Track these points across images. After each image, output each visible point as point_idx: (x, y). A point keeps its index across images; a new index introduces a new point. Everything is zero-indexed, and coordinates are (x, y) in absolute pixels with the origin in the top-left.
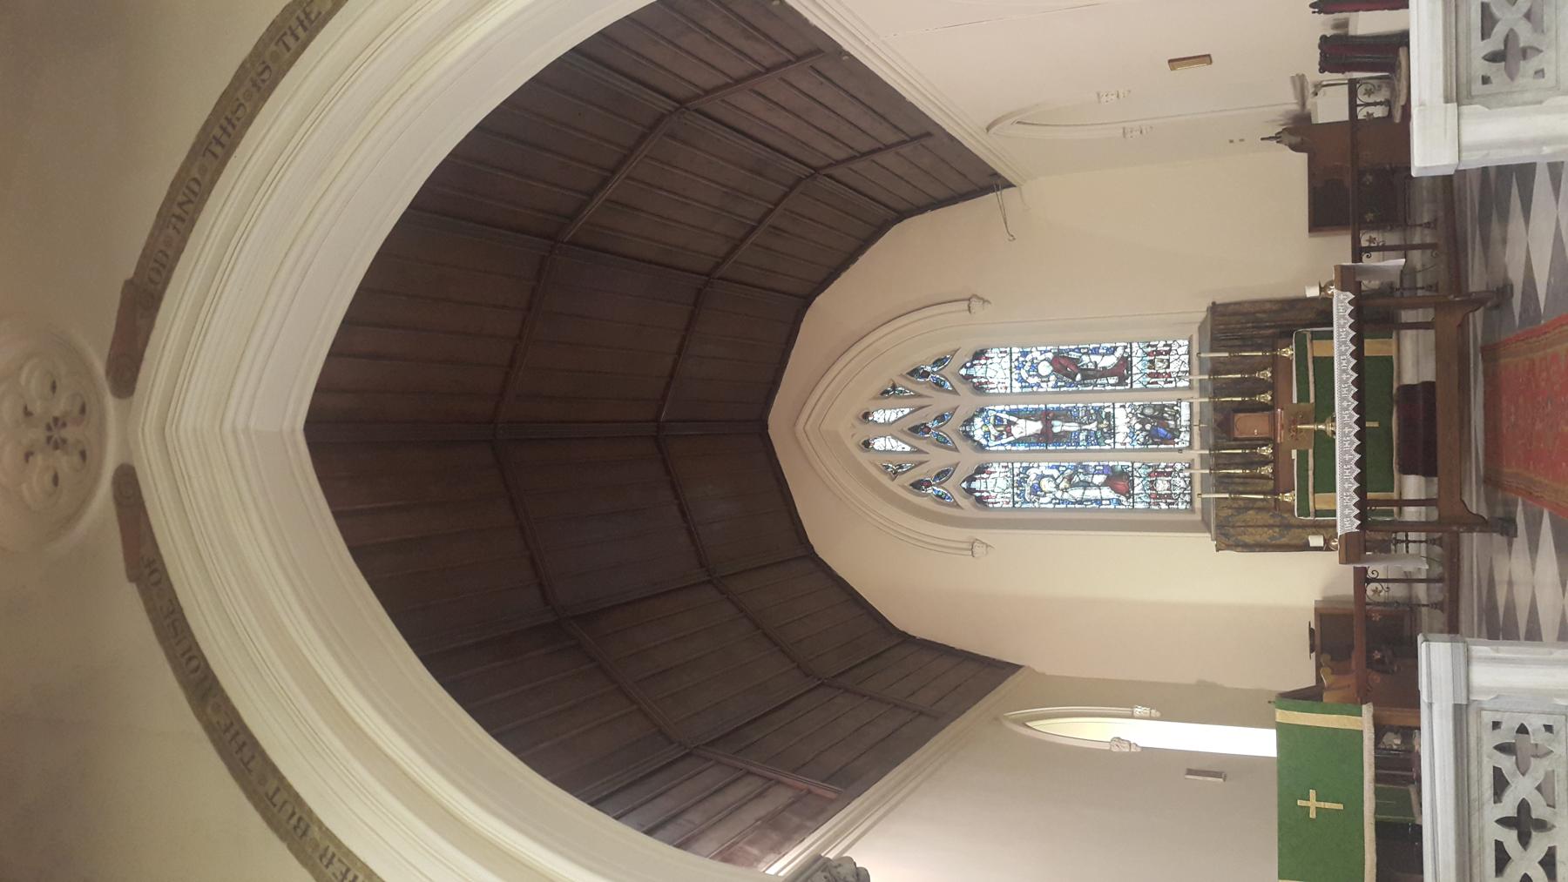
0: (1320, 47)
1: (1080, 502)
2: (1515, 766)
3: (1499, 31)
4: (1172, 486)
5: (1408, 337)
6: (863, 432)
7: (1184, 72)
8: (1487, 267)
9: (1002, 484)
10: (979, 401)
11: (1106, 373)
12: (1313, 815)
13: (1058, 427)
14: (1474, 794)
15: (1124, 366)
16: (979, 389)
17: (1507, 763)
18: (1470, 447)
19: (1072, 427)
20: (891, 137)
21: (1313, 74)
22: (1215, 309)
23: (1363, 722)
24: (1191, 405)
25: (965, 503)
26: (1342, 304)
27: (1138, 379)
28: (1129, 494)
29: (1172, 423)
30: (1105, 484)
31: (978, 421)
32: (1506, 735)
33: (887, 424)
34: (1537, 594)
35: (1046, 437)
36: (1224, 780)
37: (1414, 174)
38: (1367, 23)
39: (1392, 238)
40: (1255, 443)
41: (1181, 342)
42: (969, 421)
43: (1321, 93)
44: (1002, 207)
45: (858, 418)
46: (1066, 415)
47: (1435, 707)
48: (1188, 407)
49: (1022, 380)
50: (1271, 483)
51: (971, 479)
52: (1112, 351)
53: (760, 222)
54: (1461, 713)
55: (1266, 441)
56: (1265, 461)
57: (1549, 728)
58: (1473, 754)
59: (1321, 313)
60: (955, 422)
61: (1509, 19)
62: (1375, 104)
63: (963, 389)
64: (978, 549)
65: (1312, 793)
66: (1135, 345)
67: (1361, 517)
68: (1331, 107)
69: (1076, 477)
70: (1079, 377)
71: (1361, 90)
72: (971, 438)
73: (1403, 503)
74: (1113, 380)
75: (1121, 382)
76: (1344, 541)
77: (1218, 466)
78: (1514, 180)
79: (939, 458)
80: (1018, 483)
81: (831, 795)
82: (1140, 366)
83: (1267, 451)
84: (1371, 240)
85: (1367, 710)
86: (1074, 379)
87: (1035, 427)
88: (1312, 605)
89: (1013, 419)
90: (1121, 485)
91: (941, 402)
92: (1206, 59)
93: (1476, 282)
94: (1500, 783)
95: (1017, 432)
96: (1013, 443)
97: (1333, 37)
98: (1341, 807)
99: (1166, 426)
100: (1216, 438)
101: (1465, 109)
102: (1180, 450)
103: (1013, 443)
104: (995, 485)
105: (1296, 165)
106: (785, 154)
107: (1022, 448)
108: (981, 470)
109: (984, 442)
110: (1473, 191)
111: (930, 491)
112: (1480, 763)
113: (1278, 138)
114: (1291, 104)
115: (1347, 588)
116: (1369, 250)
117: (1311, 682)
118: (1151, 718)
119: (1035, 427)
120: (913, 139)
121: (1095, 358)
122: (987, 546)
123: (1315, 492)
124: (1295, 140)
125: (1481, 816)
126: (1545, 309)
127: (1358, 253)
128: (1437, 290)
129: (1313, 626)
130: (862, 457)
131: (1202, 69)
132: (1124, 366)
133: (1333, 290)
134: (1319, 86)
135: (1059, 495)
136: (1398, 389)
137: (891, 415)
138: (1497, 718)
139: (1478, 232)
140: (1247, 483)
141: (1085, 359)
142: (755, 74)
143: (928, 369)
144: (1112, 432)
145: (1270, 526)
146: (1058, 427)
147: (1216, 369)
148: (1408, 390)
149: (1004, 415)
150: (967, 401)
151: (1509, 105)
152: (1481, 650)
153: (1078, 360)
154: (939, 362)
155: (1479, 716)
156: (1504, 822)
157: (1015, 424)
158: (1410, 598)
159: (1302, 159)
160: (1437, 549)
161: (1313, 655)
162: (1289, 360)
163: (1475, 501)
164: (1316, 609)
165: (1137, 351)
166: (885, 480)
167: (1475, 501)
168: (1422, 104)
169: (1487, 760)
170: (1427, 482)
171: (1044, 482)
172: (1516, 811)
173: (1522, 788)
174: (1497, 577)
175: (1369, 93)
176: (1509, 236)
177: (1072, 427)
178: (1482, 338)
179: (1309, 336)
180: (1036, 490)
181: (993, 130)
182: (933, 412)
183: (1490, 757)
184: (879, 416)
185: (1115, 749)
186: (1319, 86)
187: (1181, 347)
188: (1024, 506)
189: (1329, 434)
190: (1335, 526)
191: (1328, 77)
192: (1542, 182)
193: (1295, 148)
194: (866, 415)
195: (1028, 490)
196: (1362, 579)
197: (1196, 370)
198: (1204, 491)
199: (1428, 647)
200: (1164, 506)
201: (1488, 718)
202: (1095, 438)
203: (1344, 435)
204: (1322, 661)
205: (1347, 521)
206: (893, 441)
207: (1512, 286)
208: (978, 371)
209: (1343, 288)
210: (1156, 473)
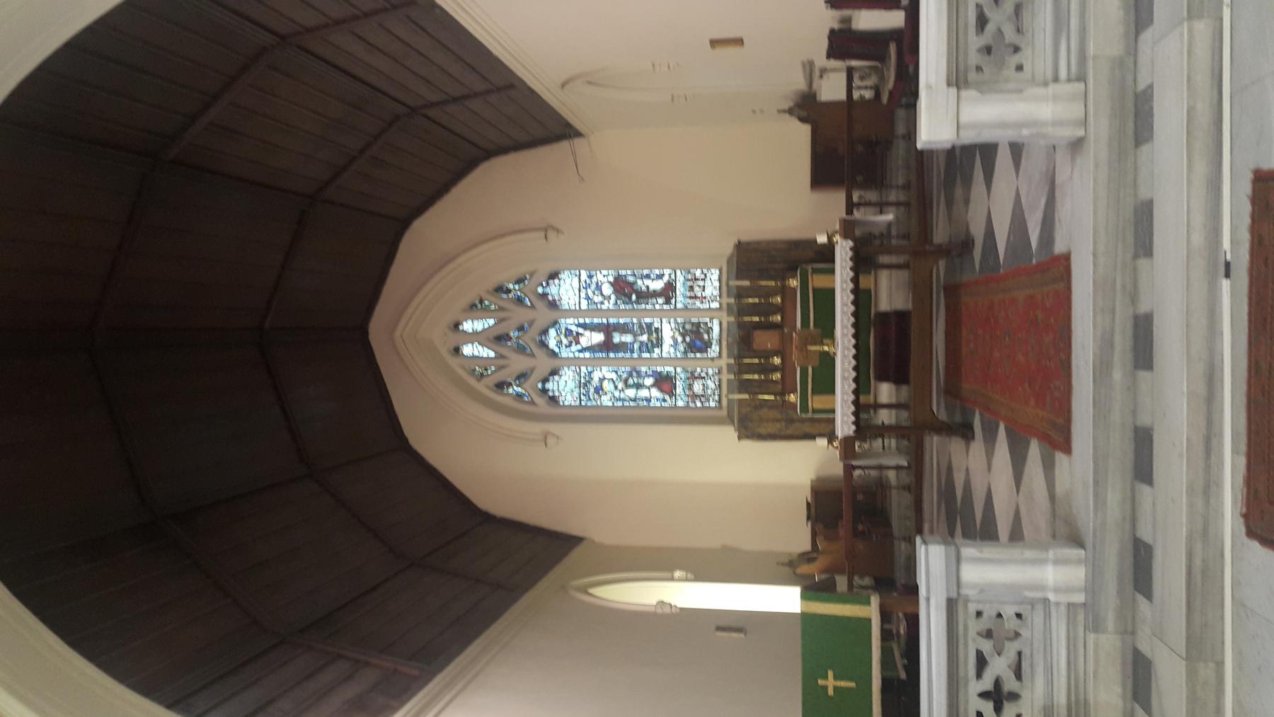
0: (829, 38)
1: (634, 400)
2: (993, 648)
3: (990, 28)
4: (705, 387)
5: (884, 276)
6: (453, 339)
7: (721, 51)
8: (950, 219)
9: (571, 385)
10: (552, 315)
11: (655, 294)
12: (831, 692)
13: (617, 338)
14: (962, 673)
15: (670, 289)
16: (554, 305)
17: (986, 646)
18: (931, 364)
19: (628, 338)
20: (479, 86)
21: (821, 60)
22: (741, 247)
23: (872, 611)
24: (721, 324)
25: (539, 400)
26: (843, 251)
27: (680, 300)
28: (671, 392)
29: (706, 337)
30: (653, 385)
31: (552, 332)
32: (983, 624)
33: (475, 333)
34: (953, 459)
35: (608, 346)
36: (745, 635)
37: (919, 146)
38: (869, 20)
39: (872, 196)
40: (768, 355)
41: (713, 271)
42: (545, 332)
43: (825, 77)
44: (574, 153)
45: (450, 328)
46: (624, 329)
47: (932, 601)
48: (718, 323)
49: (588, 298)
50: (780, 387)
51: (545, 381)
52: (660, 277)
53: (362, 152)
54: (952, 606)
55: (776, 353)
56: (775, 369)
57: (1019, 616)
58: (961, 641)
59: (826, 255)
60: (533, 333)
61: (997, 18)
62: (866, 88)
63: (540, 305)
64: (551, 441)
65: (830, 674)
66: (678, 272)
67: (856, 423)
68: (832, 89)
69: (632, 379)
70: (634, 297)
71: (856, 76)
72: (547, 346)
73: (877, 406)
74: (661, 301)
75: (668, 302)
76: (843, 444)
77: (740, 372)
78: (978, 152)
79: (519, 363)
80: (584, 385)
81: (415, 672)
82: (682, 290)
83: (777, 361)
84: (860, 197)
85: (875, 600)
86: (630, 298)
87: (598, 338)
88: (809, 483)
89: (581, 330)
90: (666, 387)
91: (521, 315)
92: (739, 42)
93: (940, 235)
94: (982, 662)
95: (584, 342)
96: (583, 350)
97: (841, 31)
98: (852, 685)
99: (701, 339)
100: (739, 350)
101: (964, 93)
102: (712, 359)
103: (583, 350)
104: (565, 387)
105: (801, 134)
106: (384, 93)
107: (587, 355)
108: (555, 372)
109: (557, 350)
110: (940, 164)
111: (511, 391)
112: (966, 645)
113: (790, 111)
114: (800, 84)
115: (838, 469)
116: (859, 205)
117: (807, 546)
118: (687, 580)
119: (598, 338)
120: (499, 89)
121: (647, 282)
122: (558, 438)
123: (813, 393)
124: (804, 114)
125: (966, 691)
126: (1004, 261)
127: (850, 207)
128: (909, 239)
129: (809, 500)
130: (453, 361)
131: (732, 51)
132: (670, 289)
133: (837, 238)
134: (823, 71)
135: (617, 394)
136: (875, 315)
137: (479, 325)
138: (980, 607)
139: (943, 194)
140: (764, 386)
141: (639, 282)
142: (356, 18)
143: (511, 286)
144: (659, 343)
145: (778, 421)
146: (617, 338)
147: (740, 294)
148: (883, 317)
149: (574, 328)
150: (543, 315)
151: (1002, 91)
152: (969, 551)
153: (635, 283)
154: (520, 281)
155: (966, 606)
156: (984, 695)
157: (581, 334)
158: (881, 478)
159: (806, 130)
160: (905, 443)
161: (809, 524)
162: (794, 290)
163: (939, 408)
164: (811, 488)
165: (680, 278)
166: (472, 381)
167: (939, 408)
168: (929, 87)
169: (972, 644)
170: (897, 390)
171: (605, 384)
172: (993, 686)
173: (999, 667)
174: (955, 465)
175: (862, 78)
176: (972, 198)
177: (628, 338)
178: (944, 278)
179: (810, 271)
180: (599, 390)
181: (567, 87)
182: (515, 322)
183: (974, 640)
184: (468, 326)
185: (659, 611)
186: (823, 71)
187: (714, 275)
188: (589, 404)
189: (832, 354)
190: (833, 421)
191: (834, 63)
192: (1003, 159)
193: (802, 120)
194: (456, 325)
195: (592, 390)
196: (849, 469)
197: (725, 294)
198: (730, 391)
199: (927, 551)
200: (699, 404)
201: (972, 608)
202: (649, 347)
203: (844, 356)
204: (817, 529)
205: (844, 425)
206: (480, 347)
207: (973, 241)
208: (553, 290)
209: (846, 236)
210: (693, 377)
